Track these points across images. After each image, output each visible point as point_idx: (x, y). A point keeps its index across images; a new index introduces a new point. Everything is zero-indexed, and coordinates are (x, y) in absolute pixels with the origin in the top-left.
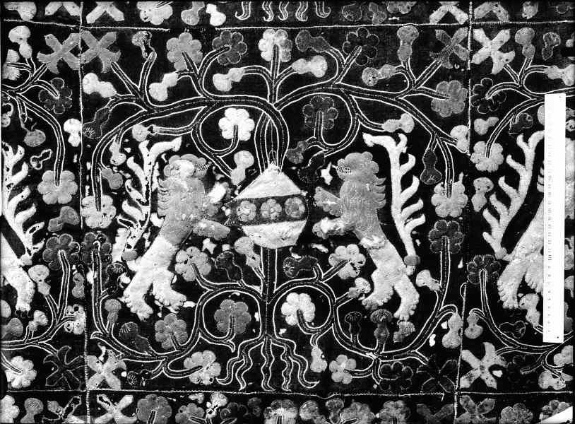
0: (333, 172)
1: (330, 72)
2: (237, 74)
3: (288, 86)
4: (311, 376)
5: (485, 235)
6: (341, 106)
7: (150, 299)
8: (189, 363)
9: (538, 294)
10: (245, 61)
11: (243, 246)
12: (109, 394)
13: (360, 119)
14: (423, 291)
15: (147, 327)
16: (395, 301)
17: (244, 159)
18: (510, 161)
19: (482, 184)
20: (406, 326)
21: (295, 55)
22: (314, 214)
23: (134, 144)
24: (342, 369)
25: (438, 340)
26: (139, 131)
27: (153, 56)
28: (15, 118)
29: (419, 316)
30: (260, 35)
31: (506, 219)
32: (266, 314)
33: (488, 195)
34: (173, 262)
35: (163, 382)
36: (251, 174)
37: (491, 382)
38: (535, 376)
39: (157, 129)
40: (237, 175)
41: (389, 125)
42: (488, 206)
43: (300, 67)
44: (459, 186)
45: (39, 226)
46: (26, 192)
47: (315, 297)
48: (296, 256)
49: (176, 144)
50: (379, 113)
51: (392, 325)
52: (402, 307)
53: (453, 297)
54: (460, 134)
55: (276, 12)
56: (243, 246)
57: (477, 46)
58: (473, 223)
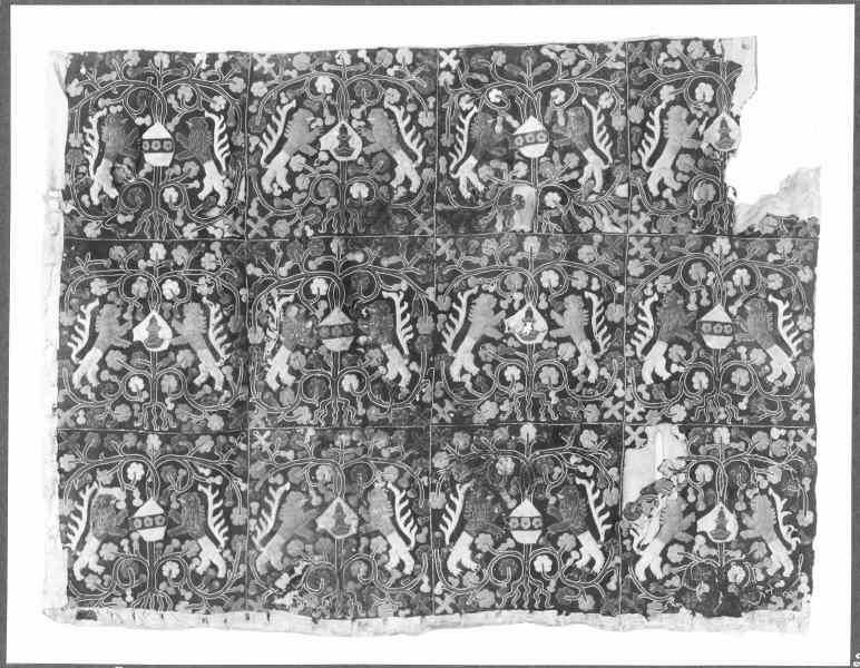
0: (367, 311)
1: (365, 260)
2: (320, 260)
3: (344, 267)
4: (358, 417)
5: (443, 344)
6: (371, 277)
7: (278, 379)
8: (296, 413)
9: (678, 171)
10: (325, 253)
11: (322, 350)
12: (260, 430)
13: (381, 284)
14: (413, 372)
15: (277, 395)
16: (399, 378)
17: (323, 305)
18: (454, 306)
19: (441, 317)
20: (405, 391)
21: (347, 251)
22: (358, 333)
23: (272, 299)
24: (373, 413)
25: (421, 397)
26: (274, 292)
27: (280, 254)
28: (215, 290)
29: (411, 386)
30: (331, 240)
31: (453, 336)
32: (334, 385)
33: (444, 324)
34: (289, 359)
35: (283, 424)
36: (327, 312)
37: (448, 420)
38: (471, 416)
39: (283, 291)
40: (319, 313)
41: (395, 287)
42: (445, 329)
43: (350, 257)
44: (430, 318)
45: (228, 345)
46: (222, 328)
47: (359, 377)
48: (349, 355)
49: (291, 299)
50: (391, 281)
51: (398, 390)
52: (402, 381)
53: (429, 377)
54: (430, 291)
55: (339, 229)
56: (322, 350)
57: (438, 247)
58: (437, 338)
